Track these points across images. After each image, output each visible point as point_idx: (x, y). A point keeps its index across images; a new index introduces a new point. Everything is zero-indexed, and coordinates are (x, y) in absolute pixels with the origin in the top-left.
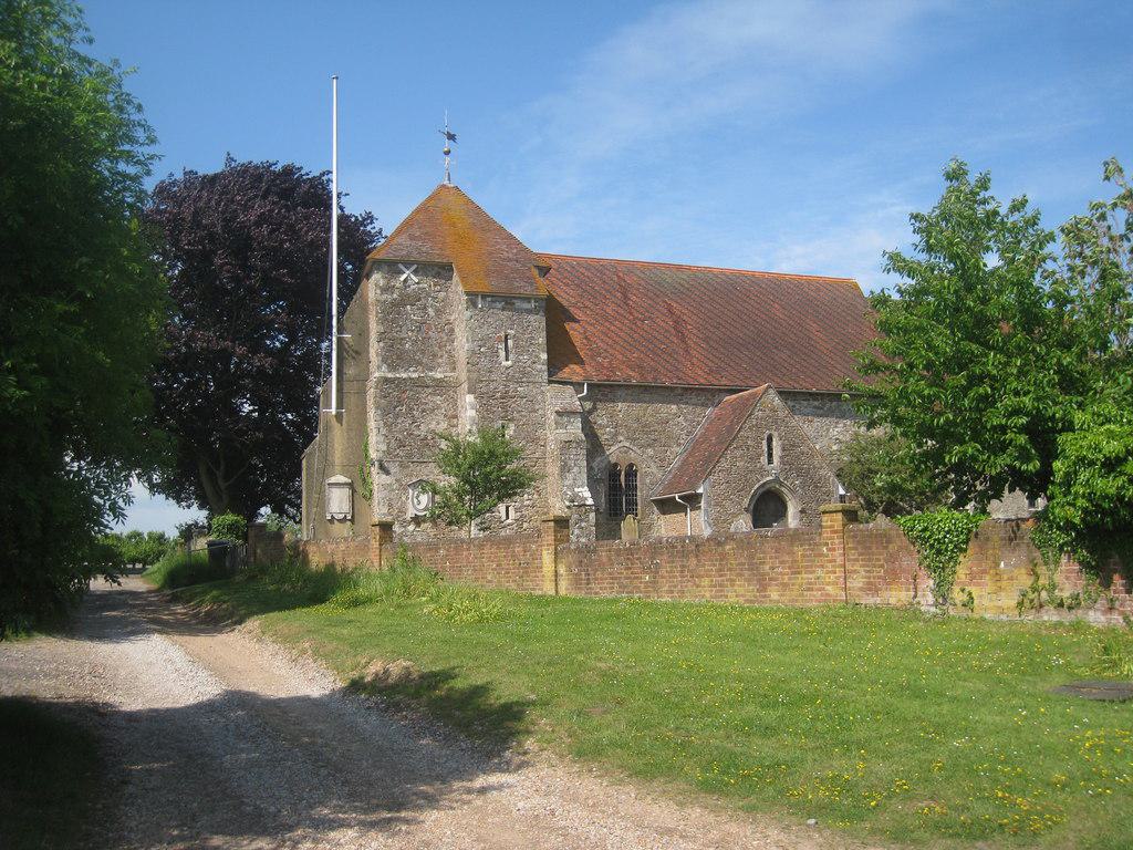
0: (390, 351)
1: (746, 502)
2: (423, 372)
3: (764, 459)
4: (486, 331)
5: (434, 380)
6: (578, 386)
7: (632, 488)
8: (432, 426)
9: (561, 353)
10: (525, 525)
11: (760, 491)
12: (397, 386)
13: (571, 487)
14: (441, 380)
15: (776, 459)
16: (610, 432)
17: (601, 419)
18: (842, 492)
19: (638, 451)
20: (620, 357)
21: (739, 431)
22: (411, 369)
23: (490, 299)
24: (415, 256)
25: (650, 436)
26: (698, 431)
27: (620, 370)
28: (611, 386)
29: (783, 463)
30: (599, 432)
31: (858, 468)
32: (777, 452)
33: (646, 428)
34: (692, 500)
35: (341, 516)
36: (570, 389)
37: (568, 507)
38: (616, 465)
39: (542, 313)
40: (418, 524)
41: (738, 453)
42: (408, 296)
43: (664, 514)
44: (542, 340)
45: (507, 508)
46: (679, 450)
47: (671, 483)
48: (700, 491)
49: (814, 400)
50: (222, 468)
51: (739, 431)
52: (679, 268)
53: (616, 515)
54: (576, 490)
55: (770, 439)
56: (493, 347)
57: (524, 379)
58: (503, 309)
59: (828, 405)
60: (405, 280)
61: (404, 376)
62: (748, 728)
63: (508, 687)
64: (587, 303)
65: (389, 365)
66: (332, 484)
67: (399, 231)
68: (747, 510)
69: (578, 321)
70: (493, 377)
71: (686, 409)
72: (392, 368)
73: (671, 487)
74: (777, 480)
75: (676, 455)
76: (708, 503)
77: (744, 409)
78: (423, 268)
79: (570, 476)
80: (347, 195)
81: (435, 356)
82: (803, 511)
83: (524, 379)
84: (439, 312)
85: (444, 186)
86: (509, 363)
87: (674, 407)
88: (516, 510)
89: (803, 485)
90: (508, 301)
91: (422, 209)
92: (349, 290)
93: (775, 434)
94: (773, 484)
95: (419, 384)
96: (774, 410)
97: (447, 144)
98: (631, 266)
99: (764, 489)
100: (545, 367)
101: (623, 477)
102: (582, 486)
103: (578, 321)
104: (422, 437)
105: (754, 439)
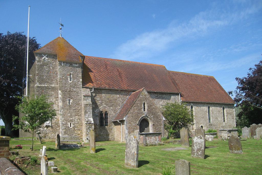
1: (138, 122)
2: (49, 85)
3: (143, 110)
4: (64, 72)
5: (52, 87)
6: (91, 89)
7: (106, 118)
8: (51, 100)
9: (86, 79)
10: (76, 129)
11: (142, 119)
13: (88, 118)
14: (54, 87)
15: (146, 110)
16: (100, 102)
17: (98, 98)
18: (164, 119)
19: (108, 108)
20: (103, 81)
21: (136, 101)
23: (65, 63)
24: (47, 52)
25: (111, 103)
26: (125, 102)
27: (103, 85)
28: (101, 89)
29: (148, 111)
30: (97, 102)
31: (32, 160)
32: (146, 108)
33: (110, 101)
34: (122, 122)
36: (89, 90)
37: (86, 124)
38: (102, 111)
39: (80, 68)
40: (47, 128)
41: (135, 108)
43: (115, 126)
44: (80, 75)
45: (71, 124)
46: (120, 107)
47: (117, 117)
48: (124, 119)
49: (156, 94)
50: (4, 112)
51: (136, 101)
52: (121, 61)
53: (102, 126)
54: (89, 119)
55: (144, 104)
57: (75, 87)
58: (69, 66)
59: (159, 96)
60: (44, 59)
61: (43, 86)
64: (96, 68)
65: (39, 83)
67: (44, 47)
68: (138, 125)
69: (93, 72)
70: (66, 86)
71: (121, 96)
72: (40, 83)
73: (117, 118)
74: (146, 116)
75: (119, 109)
76: (127, 123)
77: (137, 96)
78: (49, 56)
79: (87, 115)
81: (52, 80)
82: (153, 125)
83: (75, 87)
84: (53, 68)
85: (59, 37)
86: (71, 82)
87: (118, 95)
89: (154, 117)
90: (71, 64)
91: (53, 42)
92: (31, 63)
93: (146, 102)
94: (145, 117)
95: (47, 88)
96: (145, 95)
97: (61, 27)
98: (108, 60)
99: (143, 119)
100: (81, 83)
101: (104, 115)
102: (91, 118)
103: (93, 72)
105: (140, 104)
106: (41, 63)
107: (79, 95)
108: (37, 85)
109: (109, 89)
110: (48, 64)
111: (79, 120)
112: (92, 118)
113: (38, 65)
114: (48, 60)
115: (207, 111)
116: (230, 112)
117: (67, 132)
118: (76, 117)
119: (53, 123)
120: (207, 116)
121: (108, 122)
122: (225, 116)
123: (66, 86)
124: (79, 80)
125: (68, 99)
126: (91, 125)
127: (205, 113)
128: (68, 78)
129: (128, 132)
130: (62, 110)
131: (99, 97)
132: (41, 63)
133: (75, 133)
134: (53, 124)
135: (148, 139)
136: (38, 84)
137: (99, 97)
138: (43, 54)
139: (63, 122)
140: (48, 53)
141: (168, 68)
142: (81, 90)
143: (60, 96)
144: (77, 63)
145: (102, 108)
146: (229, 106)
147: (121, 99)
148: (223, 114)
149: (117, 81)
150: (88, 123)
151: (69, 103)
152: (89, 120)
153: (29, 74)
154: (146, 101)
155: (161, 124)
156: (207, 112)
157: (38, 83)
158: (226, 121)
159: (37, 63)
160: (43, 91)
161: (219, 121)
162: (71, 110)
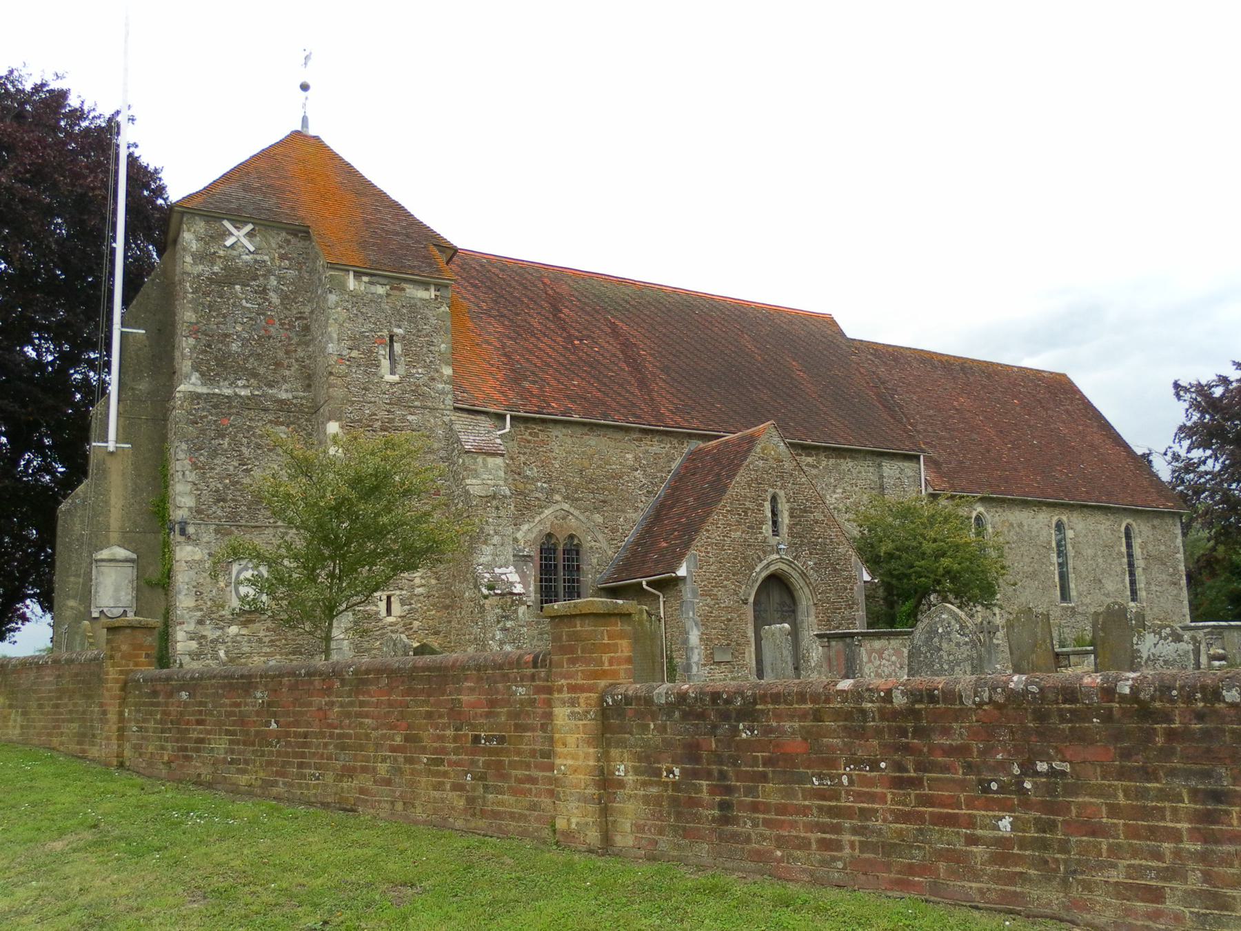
3: (767, 529)
12: (215, 406)
15: (784, 530)
18: (867, 577)
19: (581, 517)
20: (553, 382)
22: (240, 383)
29: (791, 534)
32: (785, 519)
45: (389, 598)
48: (682, 572)
49: (807, 455)
55: (774, 499)
56: (371, 352)
59: (824, 464)
62: (533, 780)
65: (202, 374)
66: (102, 560)
72: (206, 378)
88: (403, 602)
93: (781, 493)
105: (754, 500)
108: (192, 388)
112: (511, 568)
113: (199, 276)
115: (1049, 543)
116: (1162, 552)
120: (1052, 568)
122: (1139, 572)
126: (513, 601)
127: (1043, 551)
129: (701, 639)
132: (216, 269)
135: (870, 661)
136: (193, 379)
138: (228, 220)
141: (856, 327)
144: (348, 271)
145: (552, 518)
146: (1156, 522)
147: (645, 475)
148: (1125, 560)
149: (621, 385)
150: (499, 592)
152: (497, 578)
154: (783, 487)
155: (853, 603)
156: (1051, 548)
157: (195, 378)
158: (1142, 594)
159: (195, 263)
161: (1107, 595)
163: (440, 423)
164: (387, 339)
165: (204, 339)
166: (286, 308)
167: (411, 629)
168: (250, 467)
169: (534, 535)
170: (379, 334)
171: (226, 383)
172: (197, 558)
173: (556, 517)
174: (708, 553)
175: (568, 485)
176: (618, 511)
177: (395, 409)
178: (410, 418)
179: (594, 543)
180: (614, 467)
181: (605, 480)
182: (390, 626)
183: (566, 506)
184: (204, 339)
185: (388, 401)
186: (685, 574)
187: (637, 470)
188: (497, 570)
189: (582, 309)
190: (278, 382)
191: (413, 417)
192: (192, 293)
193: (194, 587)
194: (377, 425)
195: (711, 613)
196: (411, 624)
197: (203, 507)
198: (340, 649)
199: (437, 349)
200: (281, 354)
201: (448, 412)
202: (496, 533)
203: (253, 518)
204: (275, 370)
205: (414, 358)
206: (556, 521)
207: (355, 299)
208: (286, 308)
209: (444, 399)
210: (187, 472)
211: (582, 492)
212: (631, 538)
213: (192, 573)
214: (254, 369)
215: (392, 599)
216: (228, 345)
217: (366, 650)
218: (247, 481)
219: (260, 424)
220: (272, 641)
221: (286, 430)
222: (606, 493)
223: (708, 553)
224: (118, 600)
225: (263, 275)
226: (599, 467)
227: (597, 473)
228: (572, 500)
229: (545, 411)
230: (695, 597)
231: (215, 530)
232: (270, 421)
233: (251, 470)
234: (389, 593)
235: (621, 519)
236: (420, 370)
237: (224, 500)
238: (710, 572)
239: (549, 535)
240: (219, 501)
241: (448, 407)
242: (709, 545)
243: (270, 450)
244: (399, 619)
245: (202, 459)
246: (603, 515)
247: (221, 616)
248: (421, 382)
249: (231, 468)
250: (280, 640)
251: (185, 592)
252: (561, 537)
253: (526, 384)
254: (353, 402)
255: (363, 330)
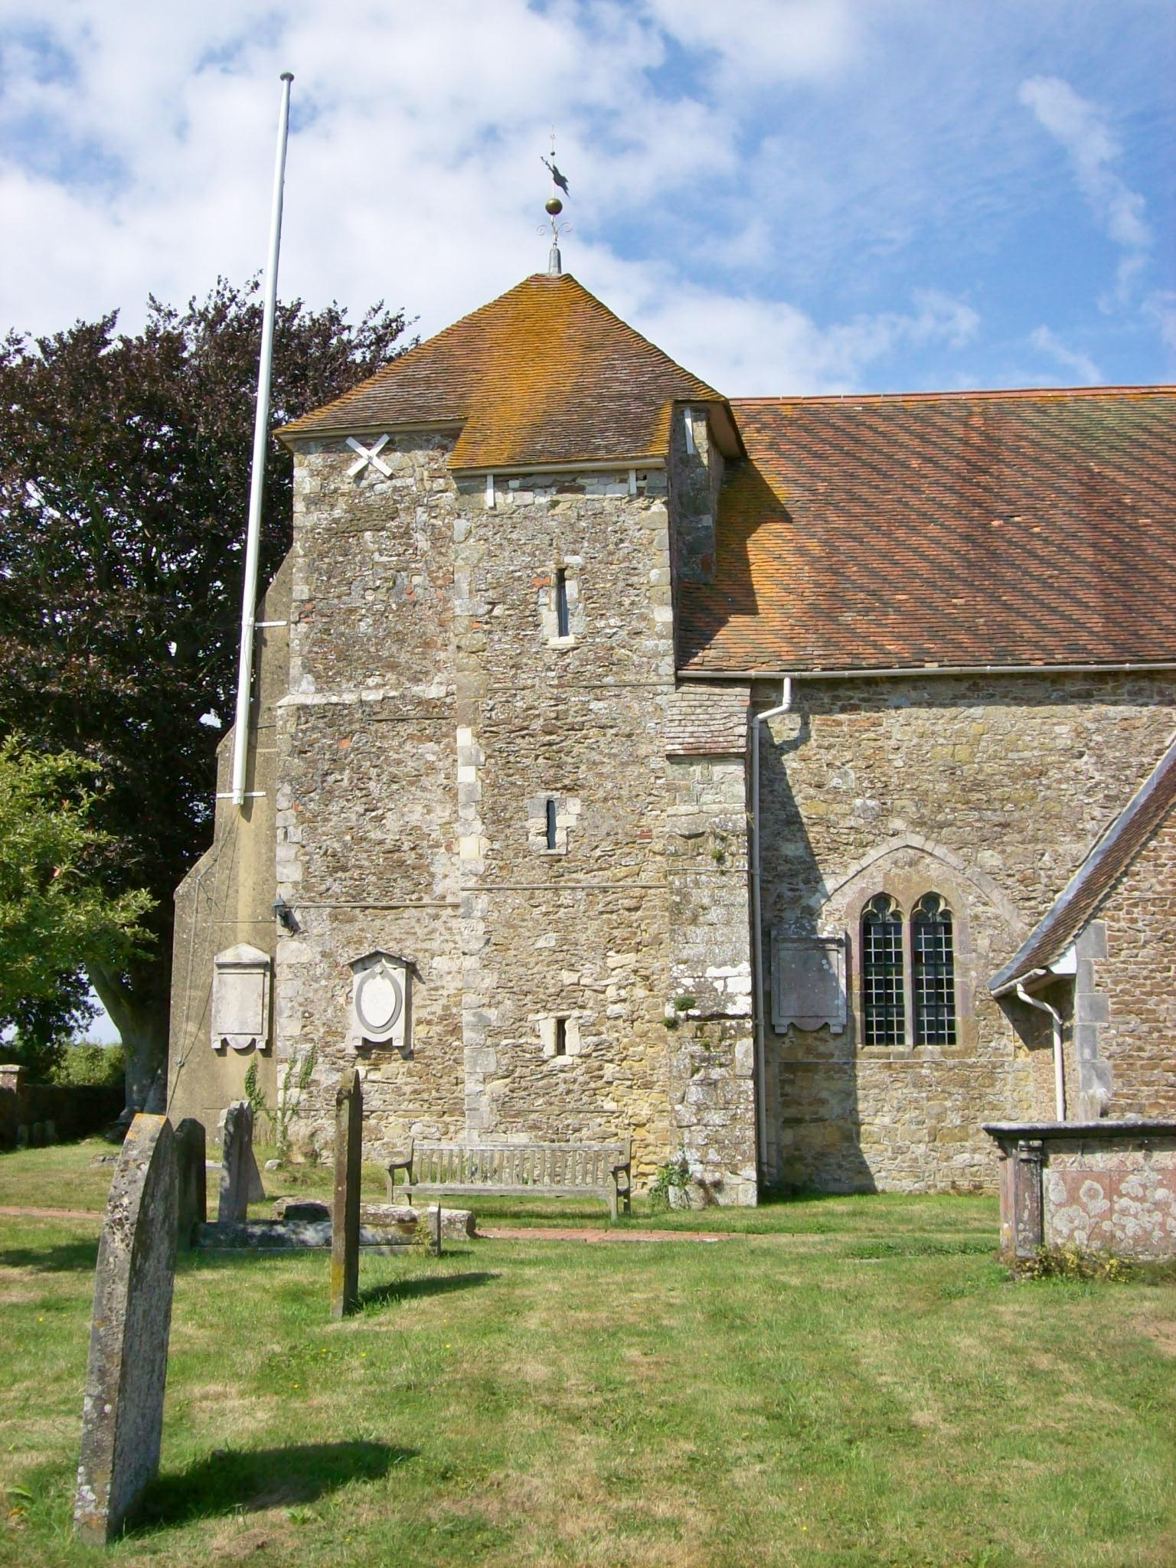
0: (320, 642)
2: (399, 684)
5: (420, 702)
8: (416, 815)
10: (609, 1070)
16: (865, 809)
22: (370, 682)
28: (869, 681)
35: (244, 1041)
42: (370, 509)
45: (561, 1023)
56: (525, 602)
61: (349, 698)
63: (127, 1544)
65: (318, 677)
70: (524, 679)
72: (324, 681)
76: (1097, 1010)
80: (152, 299)
86: (569, 640)
88: (584, 1030)
100: (667, 644)
104: (389, 845)
106: (337, 513)
107: (643, 750)
109: (958, 678)
110: (397, 511)
111: (640, 992)
114: (391, 477)
117: (519, 1105)
118: (614, 959)
119: (429, 1023)
121: (958, 1001)
123: (521, 683)
124: (643, 618)
125: (543, 795)
126: (725, 1031)
128: (543, 610)
130: (482, 902)
131: (848, 755)
132: (337, 513)
133: (600, 1111)
134: (420, 1032)
135: (1073, 1199)
136: (304, 685)
137: (848, 755)
138: (353, 436)
139: (492, 1014)
140: (389, 417)
142: (659, 708)
143: (467, 775)
144: (485, 476)
145: (886, 864)
147: (1101, 763)
151: (550, 831)
152: (704, 987)
153: (259, 615)
157: (307, 683)
159: (308, 512)
160: (346, 745)
162: (566, 898)
163: (650, 709)
164: (553, 576)
165: (320, 622)
166: (441, 553)
167: (602, 1077)
168: (380, 812)
169: (847, 900)
170: (539, 571)
171: (351, 684)
172: (304, 959)
173: (895, 863)
174: (1134, 921)
175: (922, 798)
176: (1035, 840)
177: (568, 693)
178: (594, 705)
179: (981, 909)
180: (1026, 754)
181: (1006, 781)
182: (562, 1071)
183: (917, 840)
184: (320, 622)
185: (555, 682)
186: (1073, 971)
187: (1081, 755)
188: (712, 972)
189: (1035, 460)
190: (427, 673)
191: (601, 704)
192: (305, 556)
193: (301, 1005)
194: (537, 725)
195: (1140, 1049)
196: (600, 1068)
197: (313, 880)
198: (475, 1109)
199: (643, 580)
200: (432, 628)
201: (665, 688)
202: (716, 902)
203: (386, 892)
204: (423, 653)
205: (597, 603)
206: (894, 871)
207: (497, 520)
208: (441, 553)
209: (658, 666)
210: (291, 829)
211: (953, 810)
212: (1067, 893)
213: (298, 983)
214: (392, 656)
215: (567, 1025)
216: (353, 626)
217: (518, 1114)
218: (375, 835)
219: (395, 743)
220: (415, 1092)
221: (436, 748)
222: (1009, 806)
223: (1134, 921)
224: (244, 1023)
225: (404, 510)
226: (994, 757)
227: (989, 771)
228: (932, 827)
229: (864, 663)
230: (1100, 1018)
231: (330, 915)
232: (410, 737)
233: (382, 817)
234: (560, 1014)
235: (1046, 858)
236: (612, 622)
237: (345, 869)
238: (1136, 963)
239: (882, 900)
240: (336, 870)
241: (665, 679)
242: (1136, 905)
243: (411, 783)
244: (579, 1061)
245: (312, 806)
246: (1003, 852)
247: (339, 1051)
248: (613, 642)
249: (354, 817)
250: (429, 1090)
251: (287, 1013)
252: (905, 905)
253: (848, 617)
254: (495, 691)
255: (512, 568)
